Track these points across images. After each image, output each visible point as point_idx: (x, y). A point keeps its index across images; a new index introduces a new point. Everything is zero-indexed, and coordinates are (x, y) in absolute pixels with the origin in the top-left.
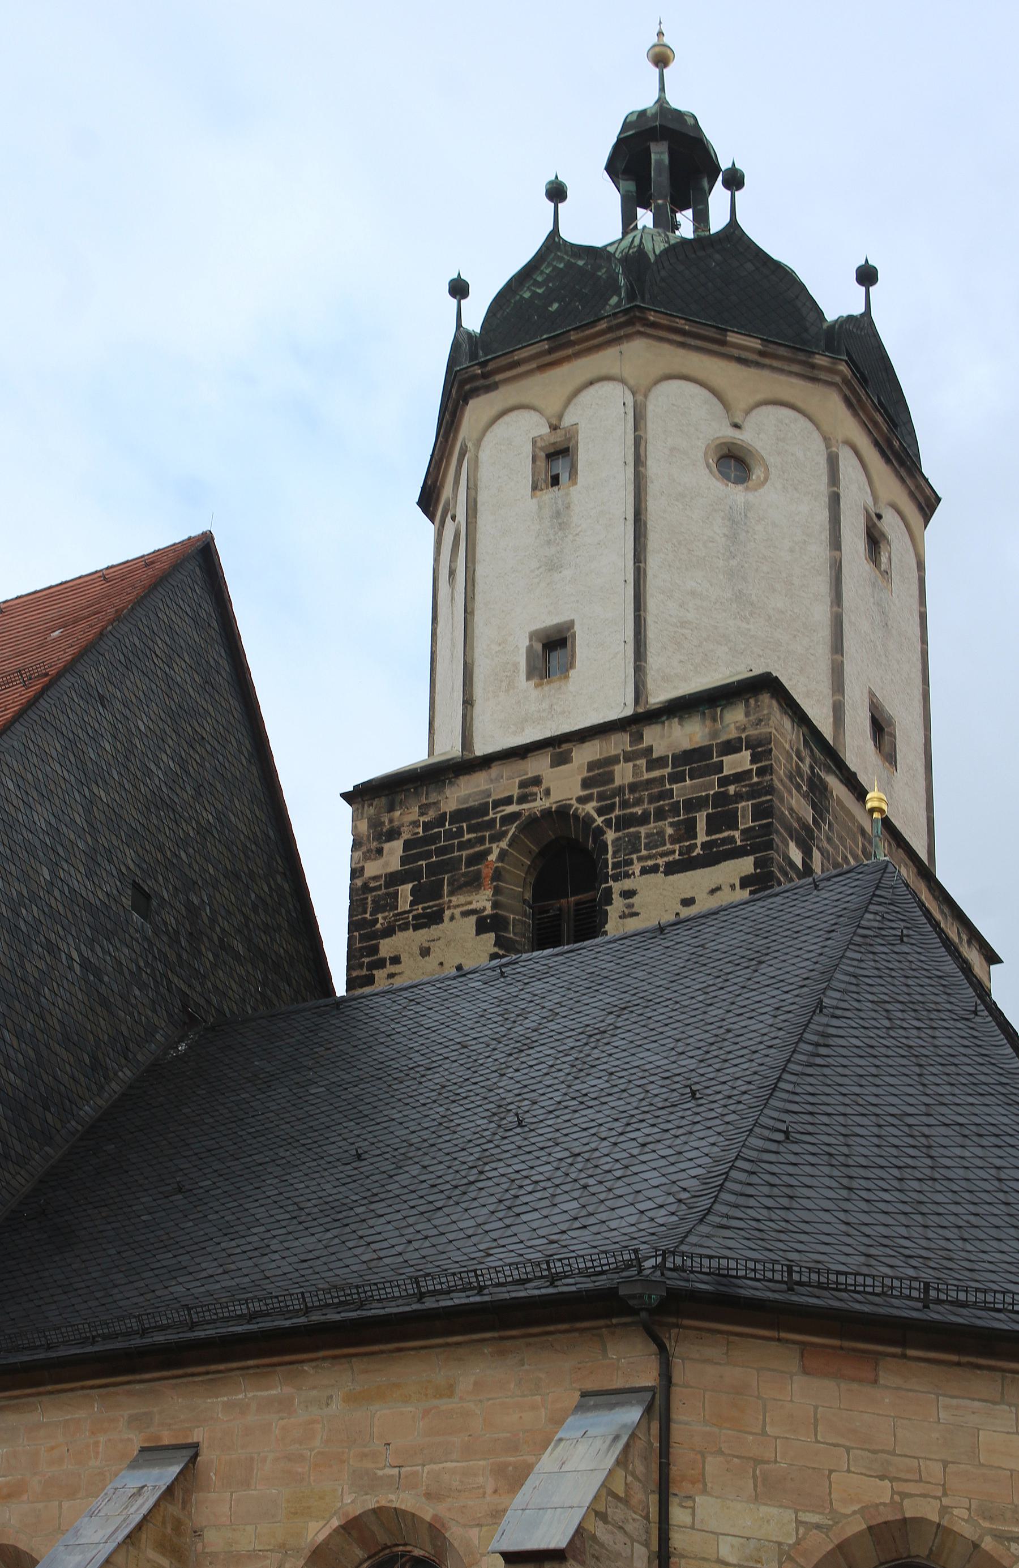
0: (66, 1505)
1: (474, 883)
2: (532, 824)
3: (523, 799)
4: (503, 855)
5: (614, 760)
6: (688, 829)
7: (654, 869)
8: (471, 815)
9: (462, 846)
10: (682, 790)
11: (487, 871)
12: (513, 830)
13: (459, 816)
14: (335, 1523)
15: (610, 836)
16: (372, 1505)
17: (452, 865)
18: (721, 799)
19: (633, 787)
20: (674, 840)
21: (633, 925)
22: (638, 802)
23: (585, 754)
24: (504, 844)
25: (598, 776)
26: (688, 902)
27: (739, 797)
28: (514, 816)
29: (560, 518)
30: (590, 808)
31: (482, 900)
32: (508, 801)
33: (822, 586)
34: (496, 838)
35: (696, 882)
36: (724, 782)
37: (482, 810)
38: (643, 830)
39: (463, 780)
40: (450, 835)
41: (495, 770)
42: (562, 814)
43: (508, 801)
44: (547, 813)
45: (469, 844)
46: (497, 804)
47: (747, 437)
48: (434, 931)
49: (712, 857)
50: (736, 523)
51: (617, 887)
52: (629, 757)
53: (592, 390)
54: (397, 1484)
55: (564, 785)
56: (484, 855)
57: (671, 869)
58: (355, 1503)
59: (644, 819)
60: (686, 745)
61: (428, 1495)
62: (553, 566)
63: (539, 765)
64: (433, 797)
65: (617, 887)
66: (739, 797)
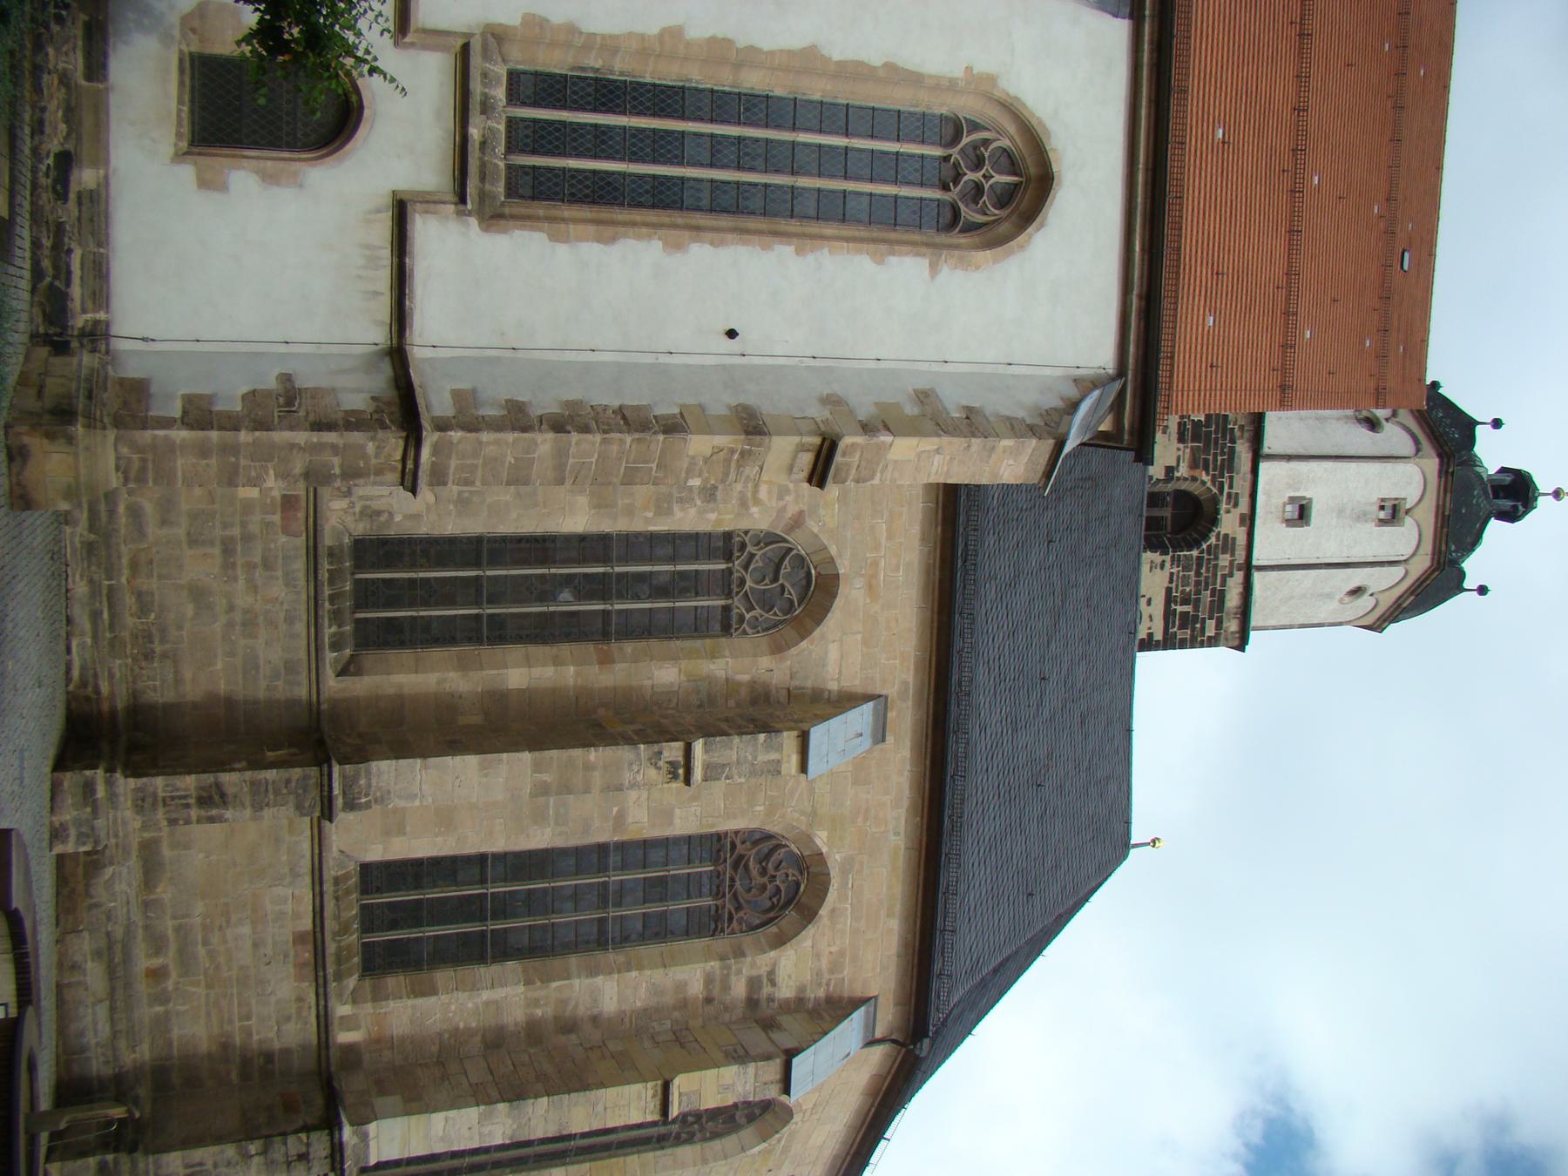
0: (859, 637)
1: (1194, 465)
2: (1215, 501)
3: (1229, 495)
4: (1204, 483)
5: (1233, 554)
6: (1185, 602)
7: (1171, 581)
8: (1230, 464)
9: (1215, 455)
10: (1206, 596)
11: (1196, 473)
12: (1215, 490)
13: (1232, 451)
14: (824, 850)
15: (1195, 553)
16: (832, 873)
17: (1206, 450)
18: (1196, 618)
19: (1216, 566)
20: (1183, 592)
21: (1145, 568)
22: (1208, 570)
23: (1241, 536)
24: (1209, 484)
25: (1228, 544)
26: (1149, 602)
27: (1193, 630)
28: (1221, 490)
29: (1361, 517)
30: (1213, 540)
31: (1183, 471)
32: (1231, 487)
33: (1287, 622)
34: (1213, 482)
35: (1158, 609)
36: (1204, 620)
37: (1231, 470)
38: (1192, 573)
39: (1250, 455)
40: (1224, 445)
41: (1249, 476)
42: (1214, 521)
43: (1231, 487)
44: (1217, 512)
45: (1215, 459)
46: (1231, 478)
47: (1366, 597)
48: (1175, 436)
49: (1168, 614)
50: (1329, 596)
51: (1168, 558)
52: (1231, 563)
53: (1415, 543)
54: (844, 885)
55: (1229, 523)
56: (1206, 469)
57: (1169, 590)
58: (835, 860)
59: (1198, 574)
60: (1228, 597)
61: (833, 910)
62: (1340, 512)
63: (1243, 506)
64: (1246, 435)
65: (1168, 558)
66: (1193, 630)
